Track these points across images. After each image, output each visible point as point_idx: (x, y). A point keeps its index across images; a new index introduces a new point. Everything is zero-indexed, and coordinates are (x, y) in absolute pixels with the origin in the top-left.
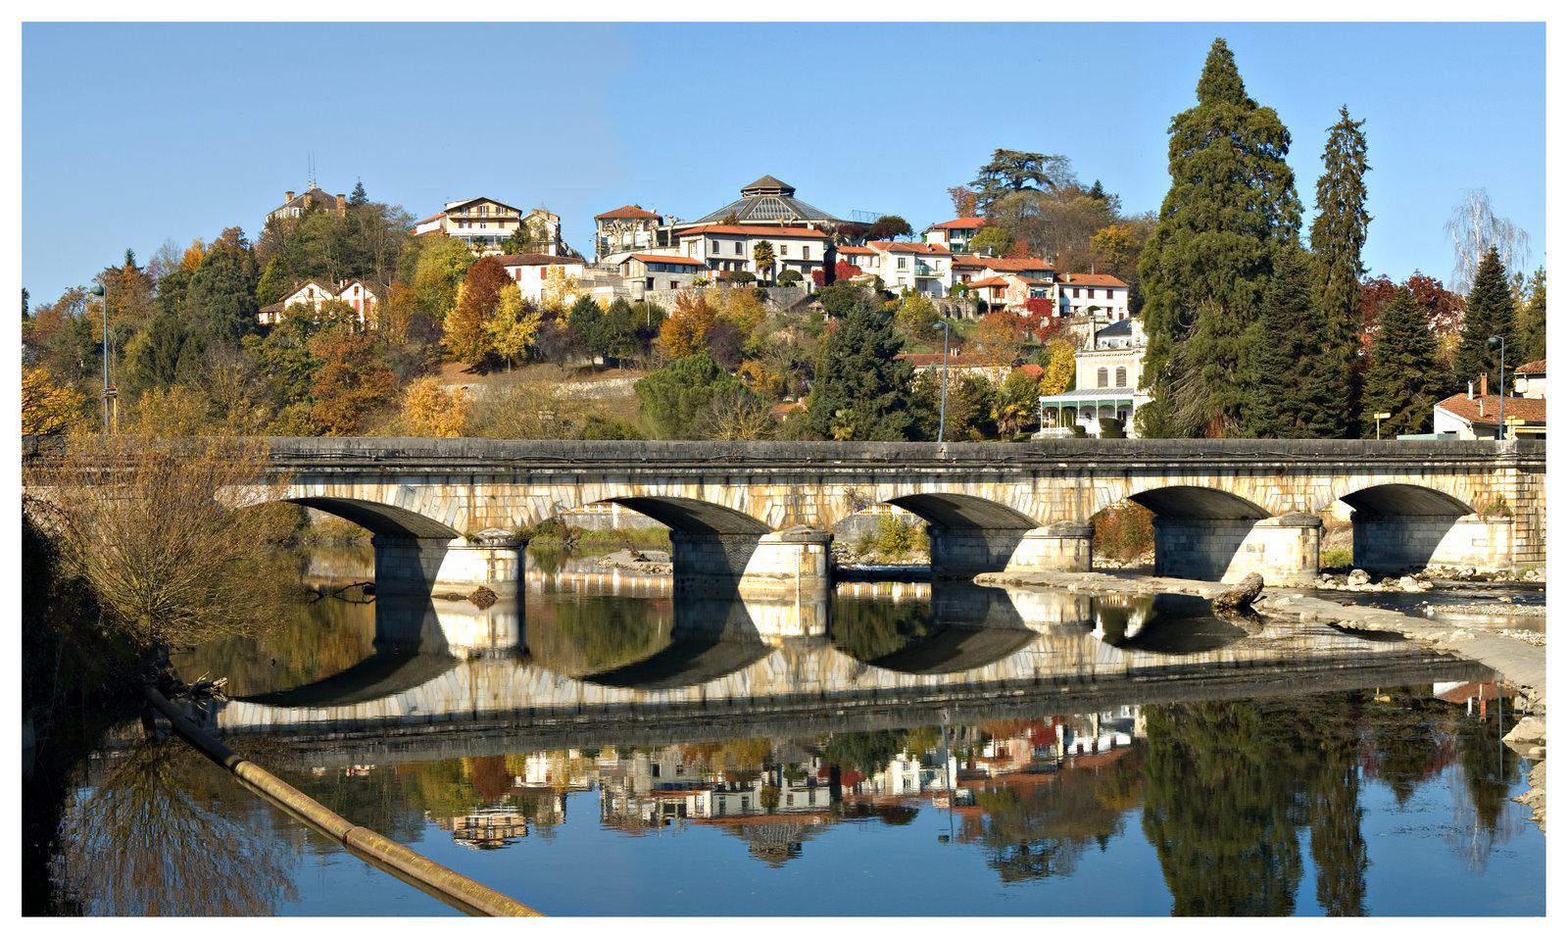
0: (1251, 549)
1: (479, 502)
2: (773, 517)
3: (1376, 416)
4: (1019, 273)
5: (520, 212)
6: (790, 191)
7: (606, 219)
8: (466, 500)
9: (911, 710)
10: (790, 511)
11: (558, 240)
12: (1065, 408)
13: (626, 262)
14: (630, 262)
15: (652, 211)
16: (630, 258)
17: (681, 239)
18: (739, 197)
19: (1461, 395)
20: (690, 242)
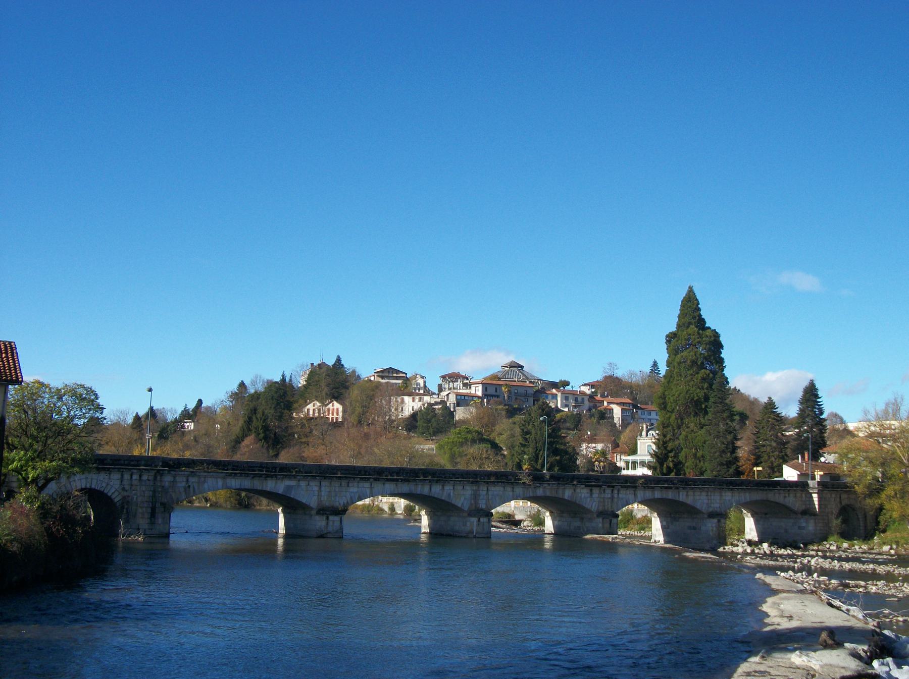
0: (661, 535)
1: (323, 493)
2: (465, 505)
3: (755, 469)
4: (617, 404)
5: (406, 374)
6: (522, 367)
7: (444, 377)
8: (317, 492)
9: (845, 521)
10: (473, 502)
11: (425, 386)
12: (632, 462)
13: (448, 395)
14: (450, 395)
15: (464, 375)
16: (450, 393)
17: (472, 385)
18: (500, 369)
19: (796, 461)
20: (476, 387)
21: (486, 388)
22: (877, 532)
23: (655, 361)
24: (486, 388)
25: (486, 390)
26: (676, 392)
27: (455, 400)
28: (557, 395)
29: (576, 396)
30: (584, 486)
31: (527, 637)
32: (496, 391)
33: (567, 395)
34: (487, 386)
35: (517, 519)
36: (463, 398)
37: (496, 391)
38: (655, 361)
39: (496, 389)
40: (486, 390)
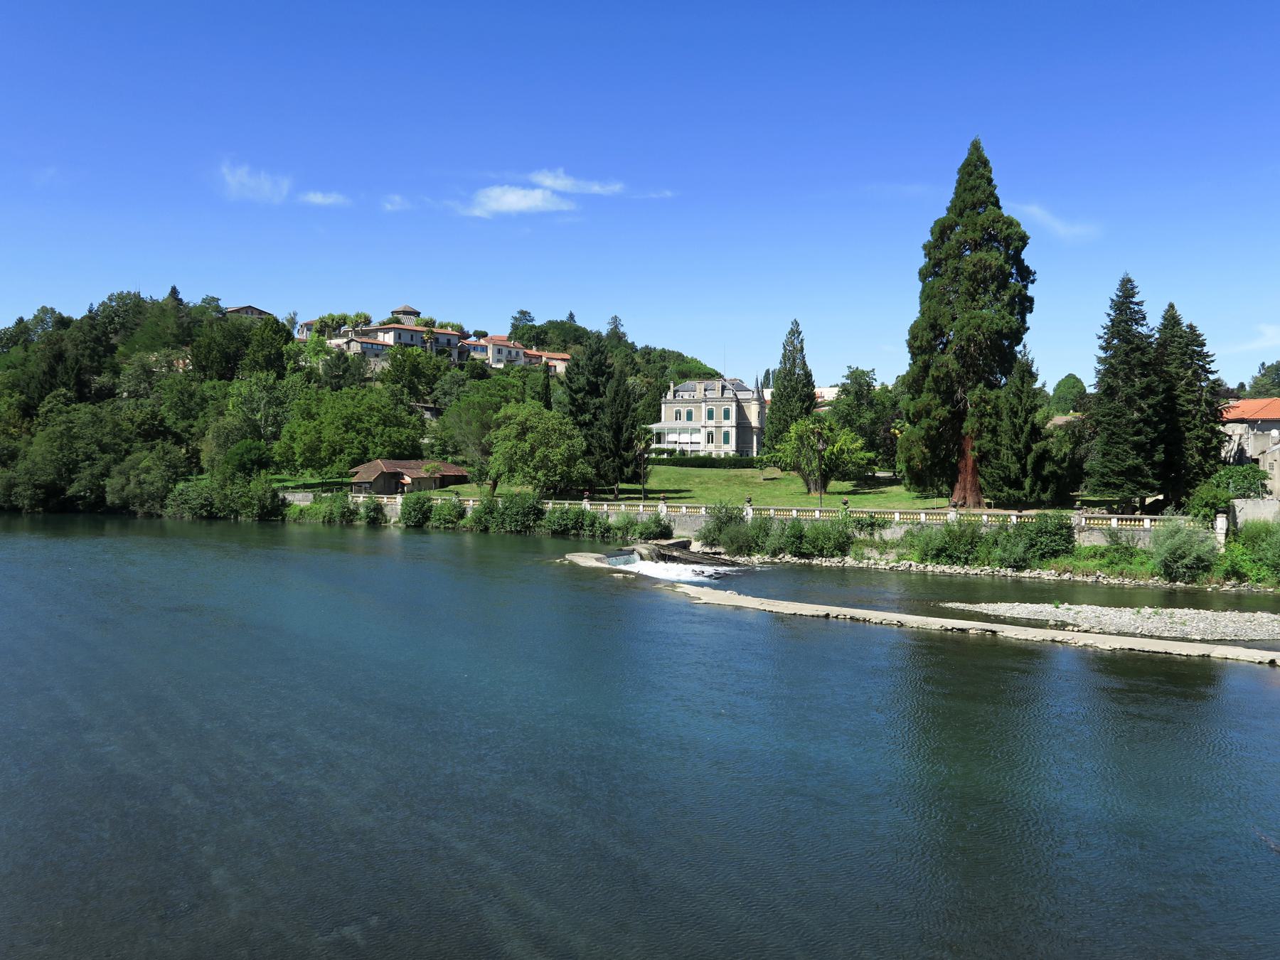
21: (400, 334)
22: (161, 437)
23: (571, 313)
24: (400, 334)
25: (400, 338)
26: (639, 924)
27: (359, 349)
28: (487, 346)
29: (510, 349)
30: (847, 485)
31: (498, 834)
32: (412, 339)
33: (500, 347)
34: (400, 331)
35: (1029, 294)
36: (370, 346)
37: (412, 339)
38: (571, 313)
39: (412, 336)
40: (400, 338)
